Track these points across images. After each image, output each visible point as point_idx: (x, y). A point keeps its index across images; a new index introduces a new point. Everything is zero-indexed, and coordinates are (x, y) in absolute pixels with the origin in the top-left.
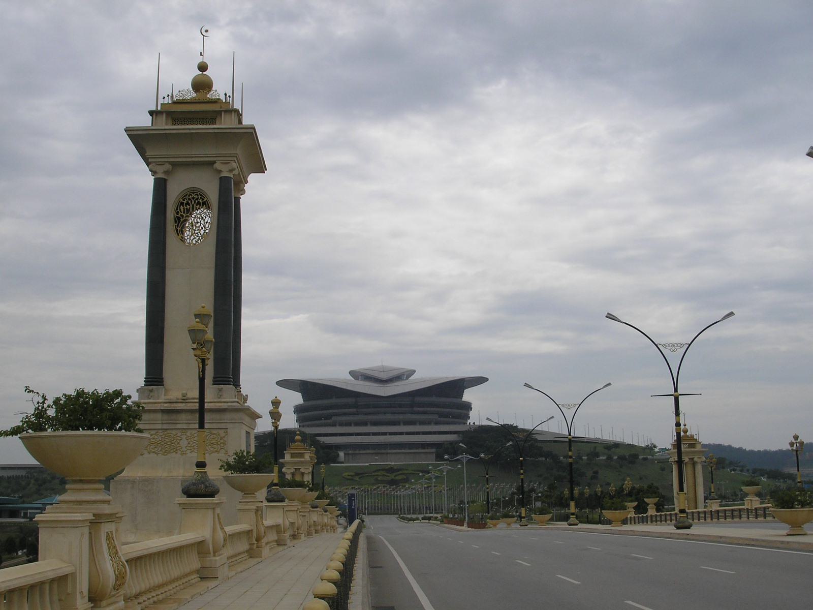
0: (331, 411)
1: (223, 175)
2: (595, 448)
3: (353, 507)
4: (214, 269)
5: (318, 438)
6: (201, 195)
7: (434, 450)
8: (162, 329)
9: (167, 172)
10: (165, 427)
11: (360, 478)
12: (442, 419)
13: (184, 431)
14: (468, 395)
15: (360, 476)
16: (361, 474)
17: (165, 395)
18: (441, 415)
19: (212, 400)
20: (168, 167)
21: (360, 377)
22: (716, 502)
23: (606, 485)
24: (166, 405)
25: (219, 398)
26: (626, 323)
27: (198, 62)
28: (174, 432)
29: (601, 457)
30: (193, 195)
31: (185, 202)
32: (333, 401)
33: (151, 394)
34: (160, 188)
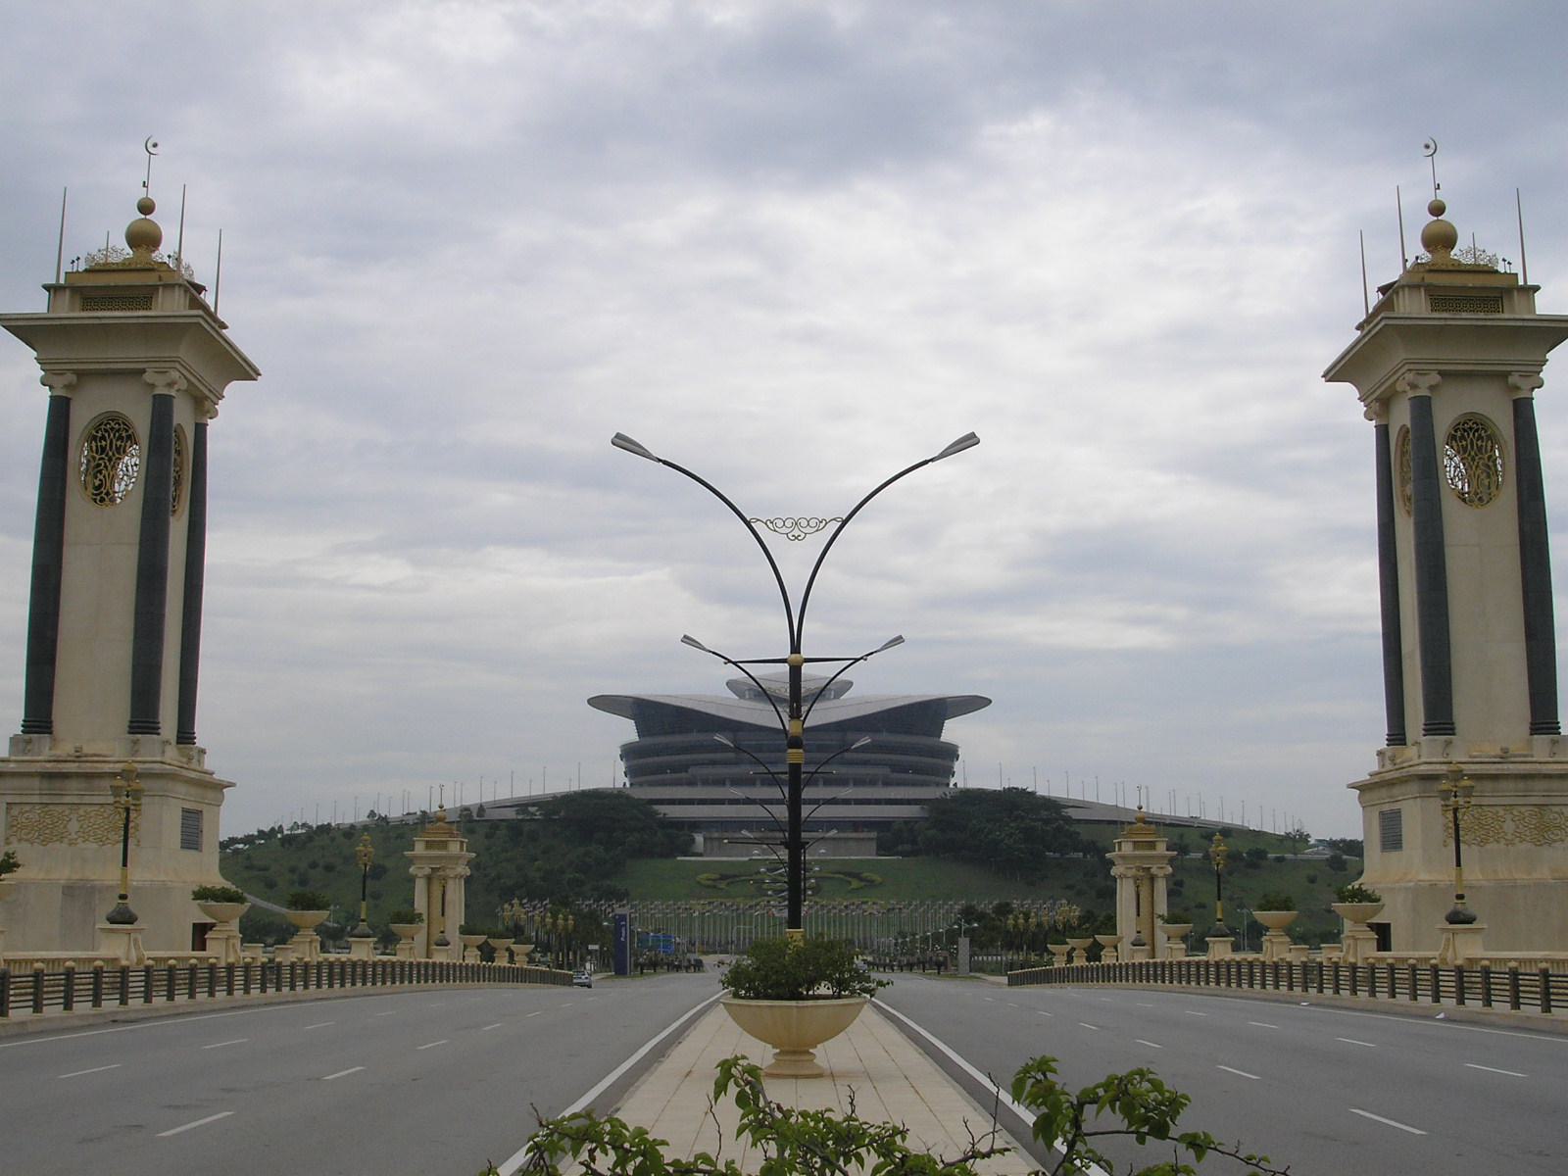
0: (688, 757)
1: (158, 391)
2: (1181, 836)
3: (622, 939)
4: (138, 547)
5: (656, 807)
6: (123, 423)
7: (873, 835)
8: (54, 642)
9: (68, 387)
10: (45, 800)
11: (728, 884)
12: (895, 775)
13: (75, 807)
14: (953, 731)
15: (728, 881)
16: (729, 877)
17: (50, 749)
18: (897, 768)
19: (122, 759)
20: (71, 378)
21: (747, 692)
22: (1143, 950)
23: (1196, 907)
24: (49, 765)
25: (133, 756)
26: (714, 653)
27: (139, 198)
28: (60, 809)
29: (1193, 855)
30: (113, 424)
31: (99, 435)
32: (694, 737)
33: (29, 747)
34: (60, 413)
